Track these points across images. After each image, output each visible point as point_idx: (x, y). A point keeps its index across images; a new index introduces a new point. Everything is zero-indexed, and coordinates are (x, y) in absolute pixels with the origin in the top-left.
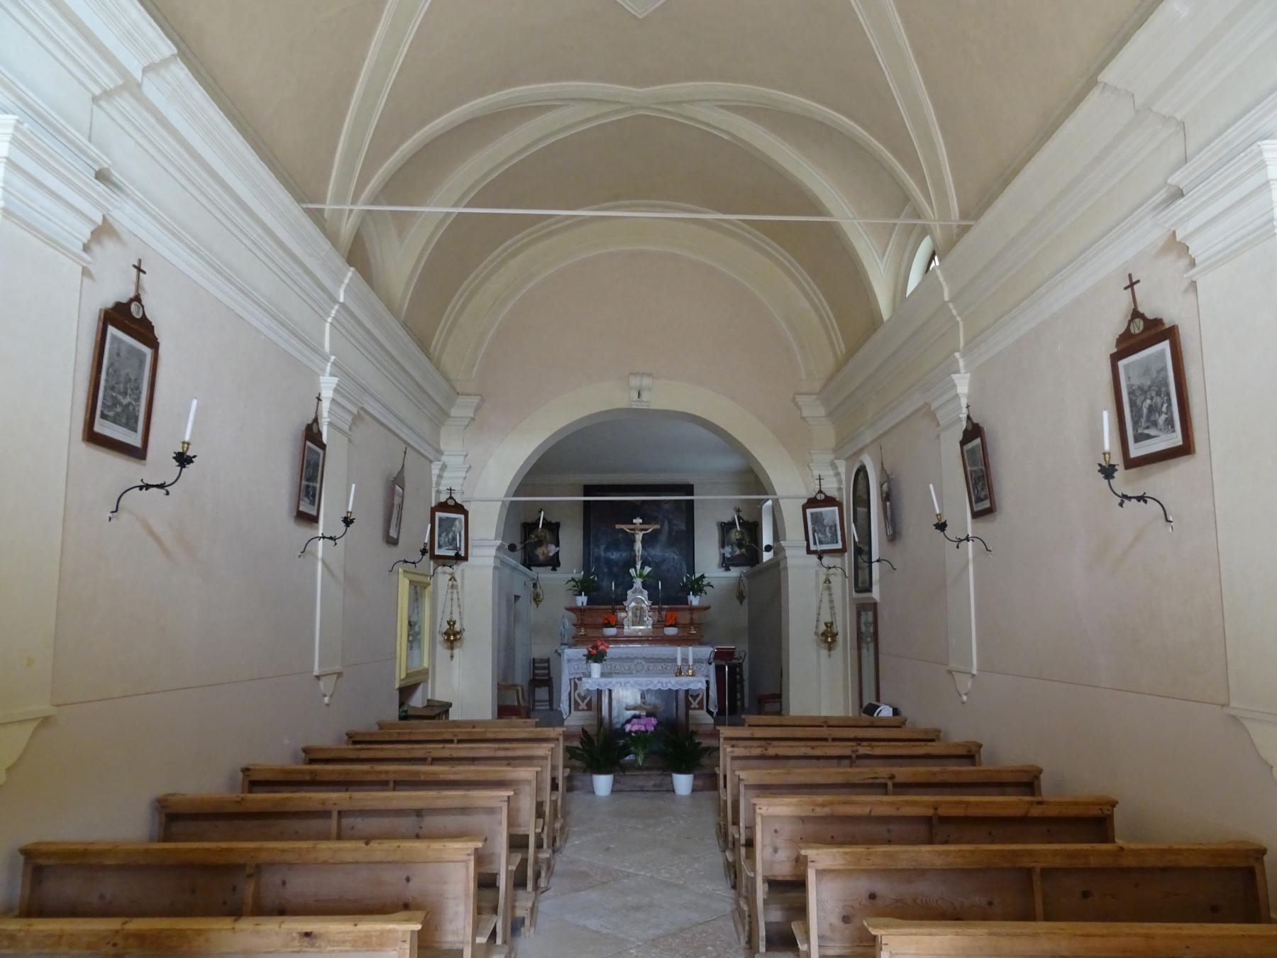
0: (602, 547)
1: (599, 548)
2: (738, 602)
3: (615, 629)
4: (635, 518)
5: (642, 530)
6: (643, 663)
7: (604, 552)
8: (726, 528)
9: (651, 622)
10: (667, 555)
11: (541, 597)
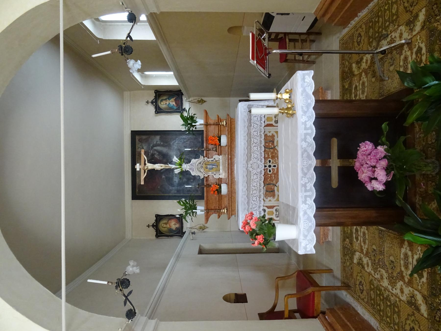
0: (171, 188)
1: (172, 190)
2: (205, 104)
3: (222, 185)
4: (136, 169)
5: (145, 164)
6: (251, 162)
7: (174, 186)
8: (158, 111)
9: (217, 156)
10: (176, 147)
11: (202, 225)
